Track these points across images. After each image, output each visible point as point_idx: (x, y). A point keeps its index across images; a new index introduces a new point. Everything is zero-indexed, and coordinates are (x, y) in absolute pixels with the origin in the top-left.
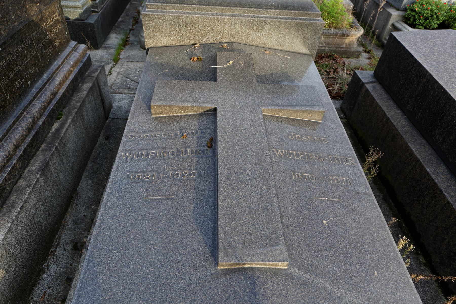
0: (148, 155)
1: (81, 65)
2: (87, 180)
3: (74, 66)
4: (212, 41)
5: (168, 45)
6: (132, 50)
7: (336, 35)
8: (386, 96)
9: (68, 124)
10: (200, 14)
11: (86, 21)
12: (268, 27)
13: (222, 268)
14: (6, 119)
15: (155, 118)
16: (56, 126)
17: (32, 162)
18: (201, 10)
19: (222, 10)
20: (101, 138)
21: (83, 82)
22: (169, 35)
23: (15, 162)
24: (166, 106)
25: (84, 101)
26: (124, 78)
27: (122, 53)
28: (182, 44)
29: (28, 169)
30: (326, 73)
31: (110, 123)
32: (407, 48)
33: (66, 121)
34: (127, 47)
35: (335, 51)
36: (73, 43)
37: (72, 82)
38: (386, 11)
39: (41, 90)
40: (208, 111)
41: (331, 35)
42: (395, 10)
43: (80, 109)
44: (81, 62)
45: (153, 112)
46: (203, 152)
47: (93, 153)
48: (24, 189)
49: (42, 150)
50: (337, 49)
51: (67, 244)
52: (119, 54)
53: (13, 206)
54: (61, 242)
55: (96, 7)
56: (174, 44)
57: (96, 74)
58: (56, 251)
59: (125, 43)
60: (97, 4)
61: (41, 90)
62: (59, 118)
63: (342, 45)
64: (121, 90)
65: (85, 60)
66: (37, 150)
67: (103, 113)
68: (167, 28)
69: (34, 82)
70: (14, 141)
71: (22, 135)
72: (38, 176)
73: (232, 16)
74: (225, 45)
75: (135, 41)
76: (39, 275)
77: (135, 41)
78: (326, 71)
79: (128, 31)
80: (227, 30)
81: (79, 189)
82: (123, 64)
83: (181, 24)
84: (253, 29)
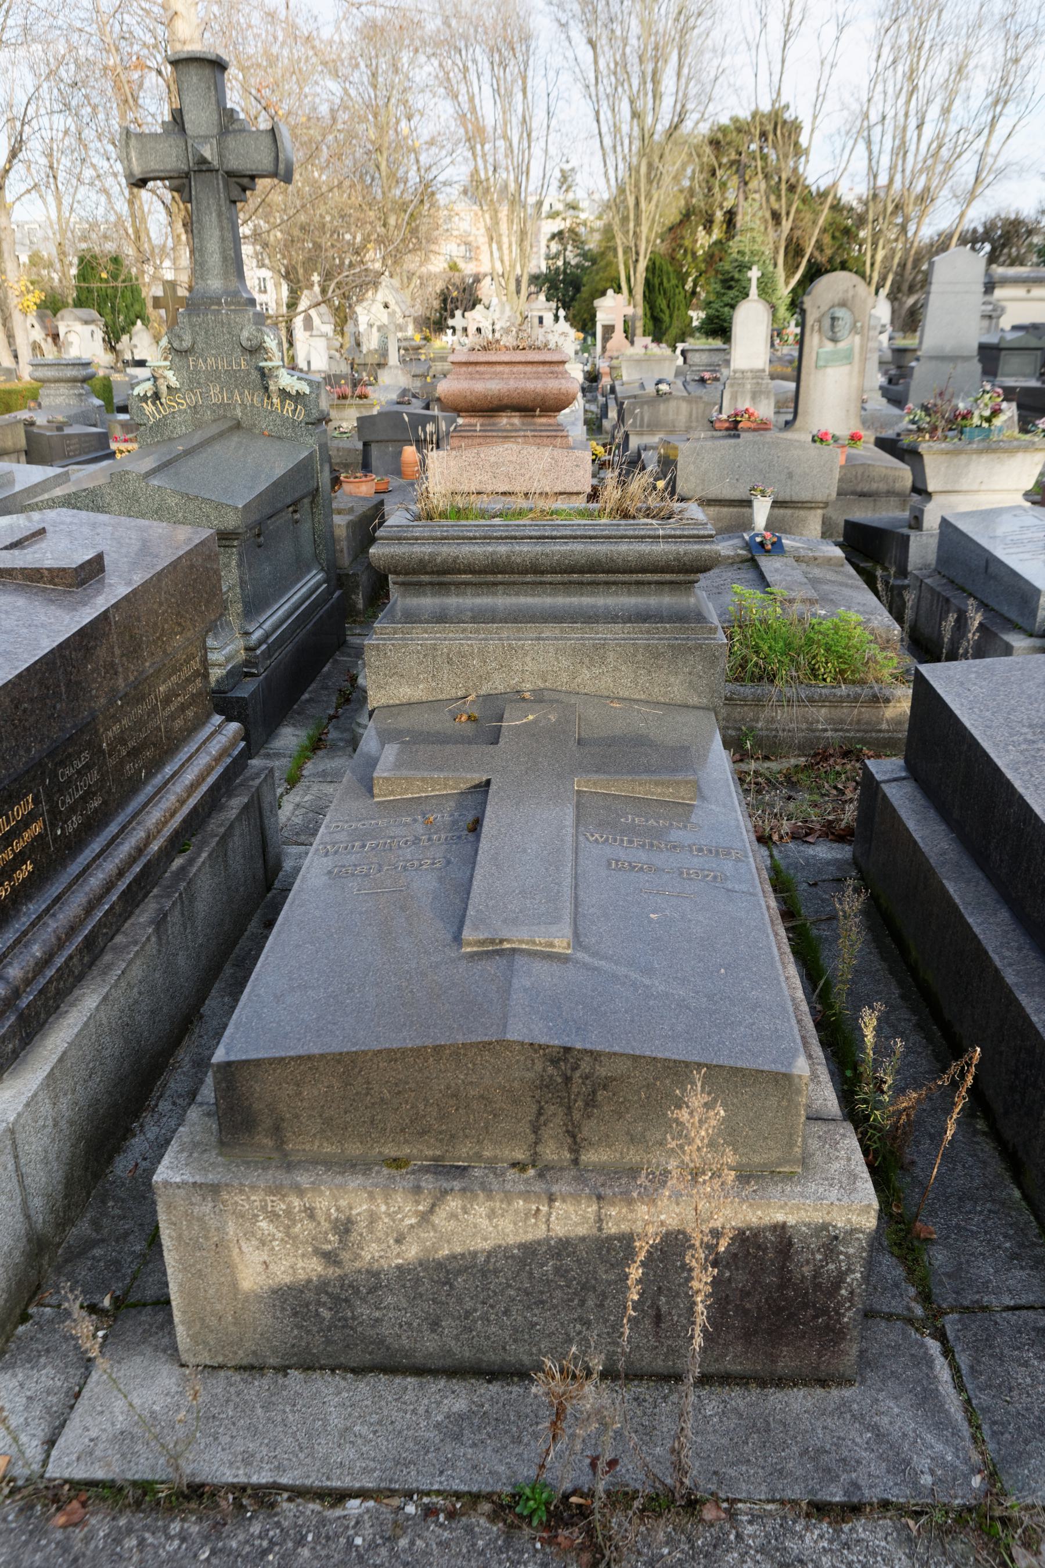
0: (364, 846)
1: (229, 760)
2: (223, 997)
3: (218, 760)
4: (501, 688)
5: (412, 700)
6: (333, 758)
7: (856, 699)
8: (922, 802)
9: (201, 860)
10: (475, 639)
11: (229, 695)
12: (611, 656)
13: (469, 950)
14: (107, 825)
15: (379, 803)
16: (178, 862)
17: (137, 912)
18: (477, 631)
19: (519, 630)
20: (253, 923)
21: (230, 795)
22: (416, 682)
23: (114, 898)
24: (400, 779)
25: (231, 826)
26: (311, 815)
27: (309, 765)
28: (440, 697)
29: (130, 922)
30: (835, 792)
31: (274, 897)
32: (939, 691)
33: (199, 855)
34: (320, 753)
35: (863, 741)
36: (217, 719)
37: (211, 789)
38: (1002, 639)
39: (160, 790)
40: (475, 787)
41: (842, 700)
42: (1022, 636)
43: (224, 839)
44: (229, 755)
45: (376, 791)
46: (459, 837)
47: (236, 950)
48: (127, 946)
49: (155, 897)
50: (868, 735)
51: (180, 1096)
52: (300, 768)
53: (109, 967)
54: (168, 1093)
55: (255, 665)
56: (424, 699)
57: (257, 782)
58: (157, 1105)
59: (316, 745)
60: (257, 657)
61: (160, 790)
62: (184, 851)
63: (879, 723)
64: (303, 837)
65: (236, 752)
66: (146, 896)
67: (262, 871)
68: (412, 668)
69: (150, 775)
70: (117, 861)
71: (130, 855)
72: (150, 930)
73: (538, 639)
74: (527, 695)
75: (341, 739)
76: (125, 1139)
77: (341, 739)
78: (835, 788)
79: (326, 721)
80: (530, 666)
81: (205, 1010)
82: (309, 787)
83: (439, 659)
84: (582, 662)
